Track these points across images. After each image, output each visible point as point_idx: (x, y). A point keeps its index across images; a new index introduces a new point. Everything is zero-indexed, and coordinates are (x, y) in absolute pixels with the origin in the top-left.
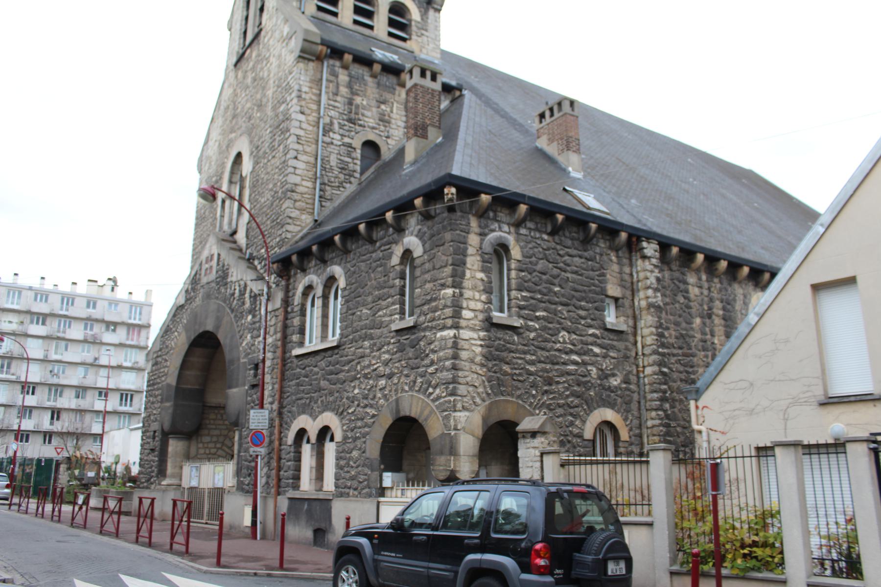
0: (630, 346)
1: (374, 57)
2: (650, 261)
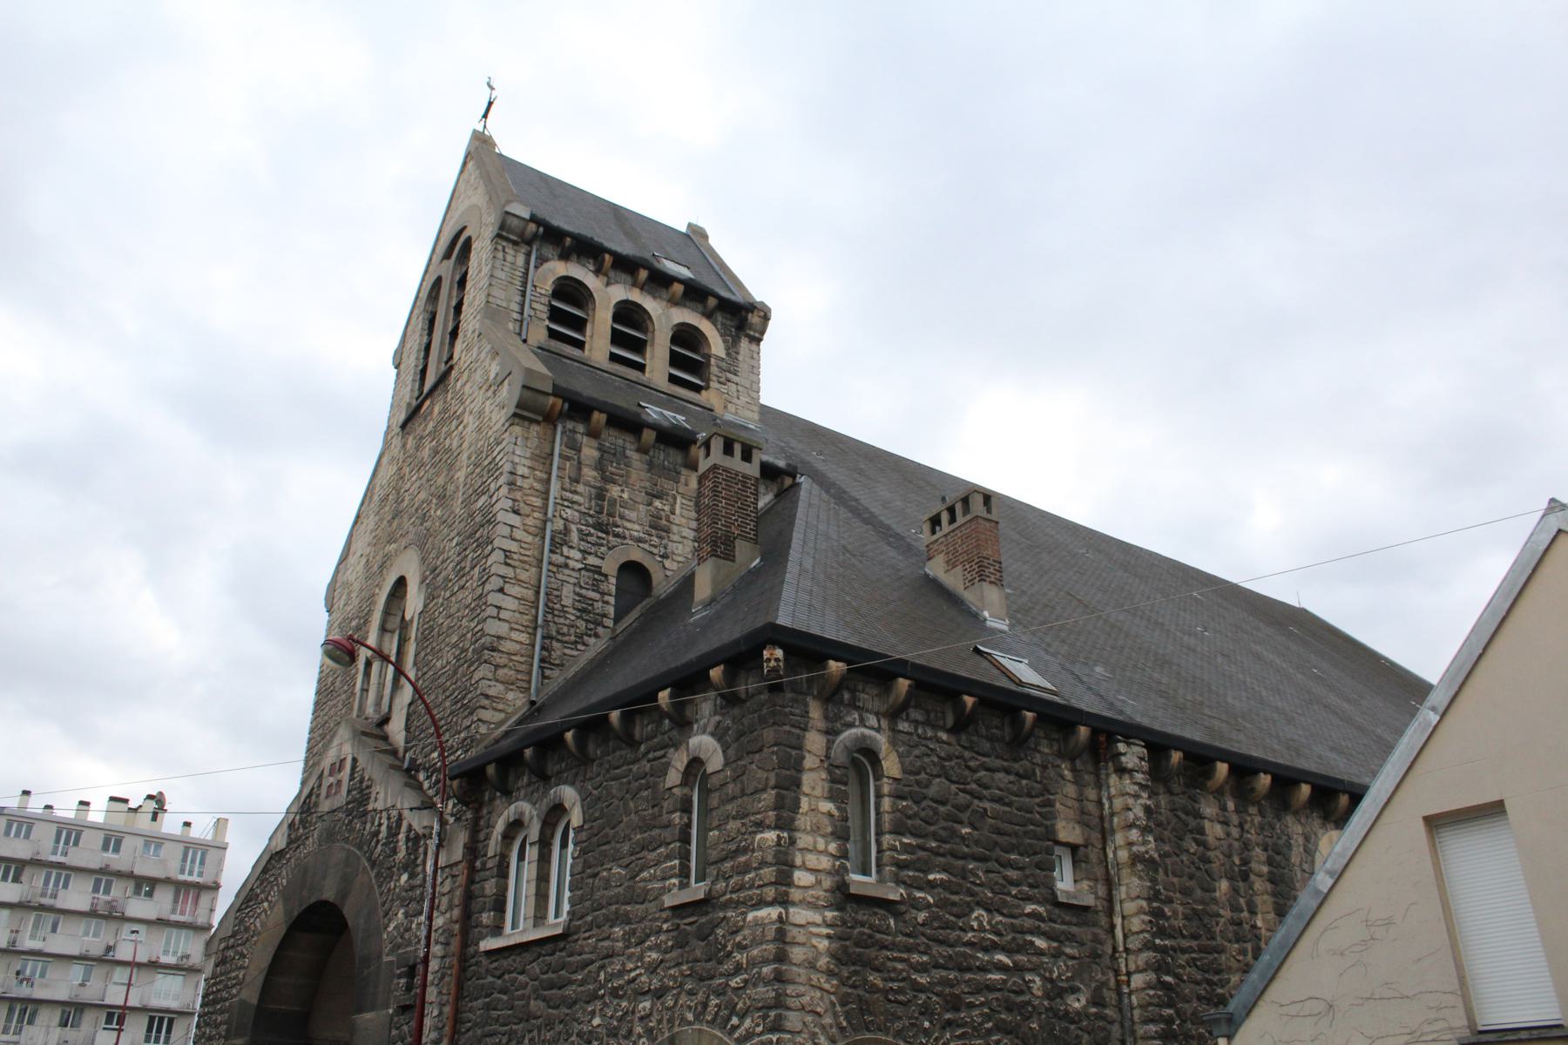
0: (1102, 935)
1: (644, 417)
2: (1132, 777)
